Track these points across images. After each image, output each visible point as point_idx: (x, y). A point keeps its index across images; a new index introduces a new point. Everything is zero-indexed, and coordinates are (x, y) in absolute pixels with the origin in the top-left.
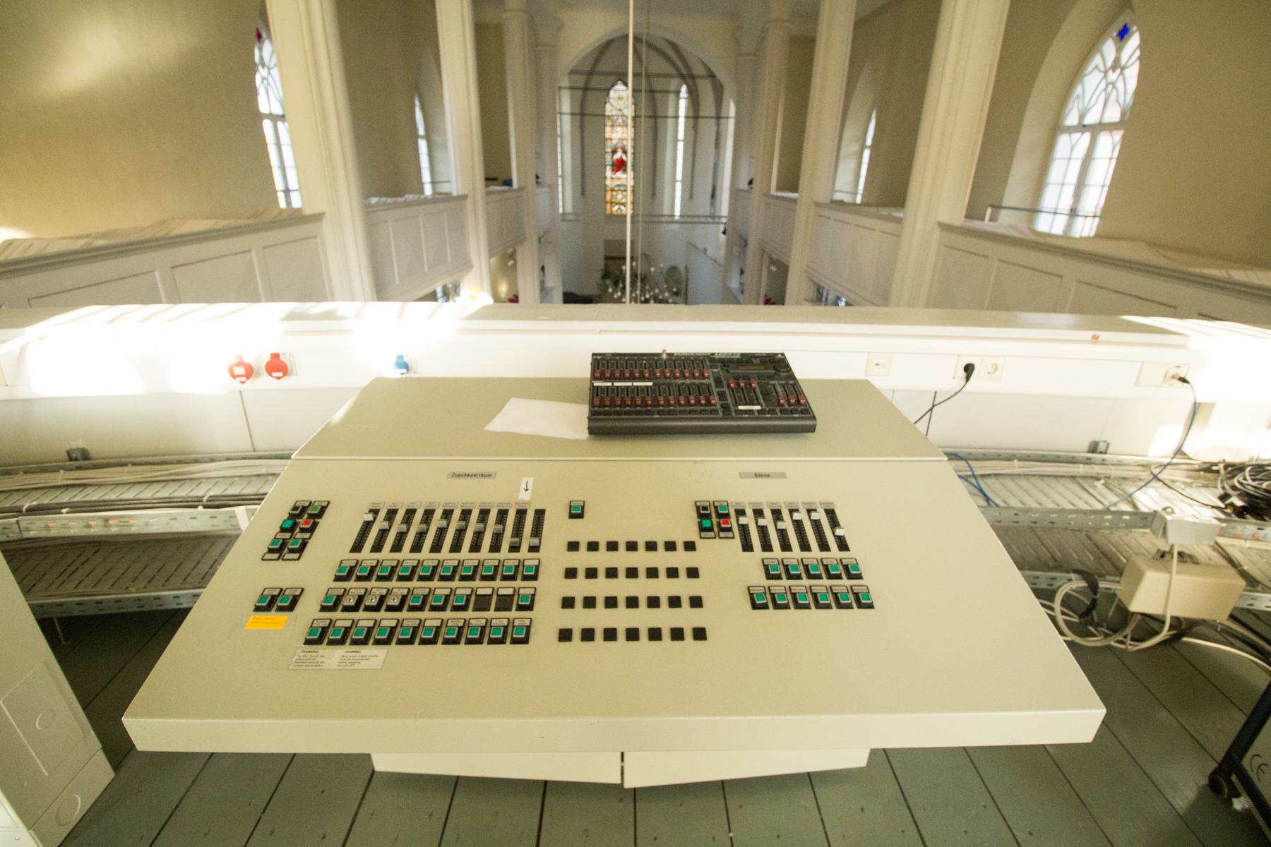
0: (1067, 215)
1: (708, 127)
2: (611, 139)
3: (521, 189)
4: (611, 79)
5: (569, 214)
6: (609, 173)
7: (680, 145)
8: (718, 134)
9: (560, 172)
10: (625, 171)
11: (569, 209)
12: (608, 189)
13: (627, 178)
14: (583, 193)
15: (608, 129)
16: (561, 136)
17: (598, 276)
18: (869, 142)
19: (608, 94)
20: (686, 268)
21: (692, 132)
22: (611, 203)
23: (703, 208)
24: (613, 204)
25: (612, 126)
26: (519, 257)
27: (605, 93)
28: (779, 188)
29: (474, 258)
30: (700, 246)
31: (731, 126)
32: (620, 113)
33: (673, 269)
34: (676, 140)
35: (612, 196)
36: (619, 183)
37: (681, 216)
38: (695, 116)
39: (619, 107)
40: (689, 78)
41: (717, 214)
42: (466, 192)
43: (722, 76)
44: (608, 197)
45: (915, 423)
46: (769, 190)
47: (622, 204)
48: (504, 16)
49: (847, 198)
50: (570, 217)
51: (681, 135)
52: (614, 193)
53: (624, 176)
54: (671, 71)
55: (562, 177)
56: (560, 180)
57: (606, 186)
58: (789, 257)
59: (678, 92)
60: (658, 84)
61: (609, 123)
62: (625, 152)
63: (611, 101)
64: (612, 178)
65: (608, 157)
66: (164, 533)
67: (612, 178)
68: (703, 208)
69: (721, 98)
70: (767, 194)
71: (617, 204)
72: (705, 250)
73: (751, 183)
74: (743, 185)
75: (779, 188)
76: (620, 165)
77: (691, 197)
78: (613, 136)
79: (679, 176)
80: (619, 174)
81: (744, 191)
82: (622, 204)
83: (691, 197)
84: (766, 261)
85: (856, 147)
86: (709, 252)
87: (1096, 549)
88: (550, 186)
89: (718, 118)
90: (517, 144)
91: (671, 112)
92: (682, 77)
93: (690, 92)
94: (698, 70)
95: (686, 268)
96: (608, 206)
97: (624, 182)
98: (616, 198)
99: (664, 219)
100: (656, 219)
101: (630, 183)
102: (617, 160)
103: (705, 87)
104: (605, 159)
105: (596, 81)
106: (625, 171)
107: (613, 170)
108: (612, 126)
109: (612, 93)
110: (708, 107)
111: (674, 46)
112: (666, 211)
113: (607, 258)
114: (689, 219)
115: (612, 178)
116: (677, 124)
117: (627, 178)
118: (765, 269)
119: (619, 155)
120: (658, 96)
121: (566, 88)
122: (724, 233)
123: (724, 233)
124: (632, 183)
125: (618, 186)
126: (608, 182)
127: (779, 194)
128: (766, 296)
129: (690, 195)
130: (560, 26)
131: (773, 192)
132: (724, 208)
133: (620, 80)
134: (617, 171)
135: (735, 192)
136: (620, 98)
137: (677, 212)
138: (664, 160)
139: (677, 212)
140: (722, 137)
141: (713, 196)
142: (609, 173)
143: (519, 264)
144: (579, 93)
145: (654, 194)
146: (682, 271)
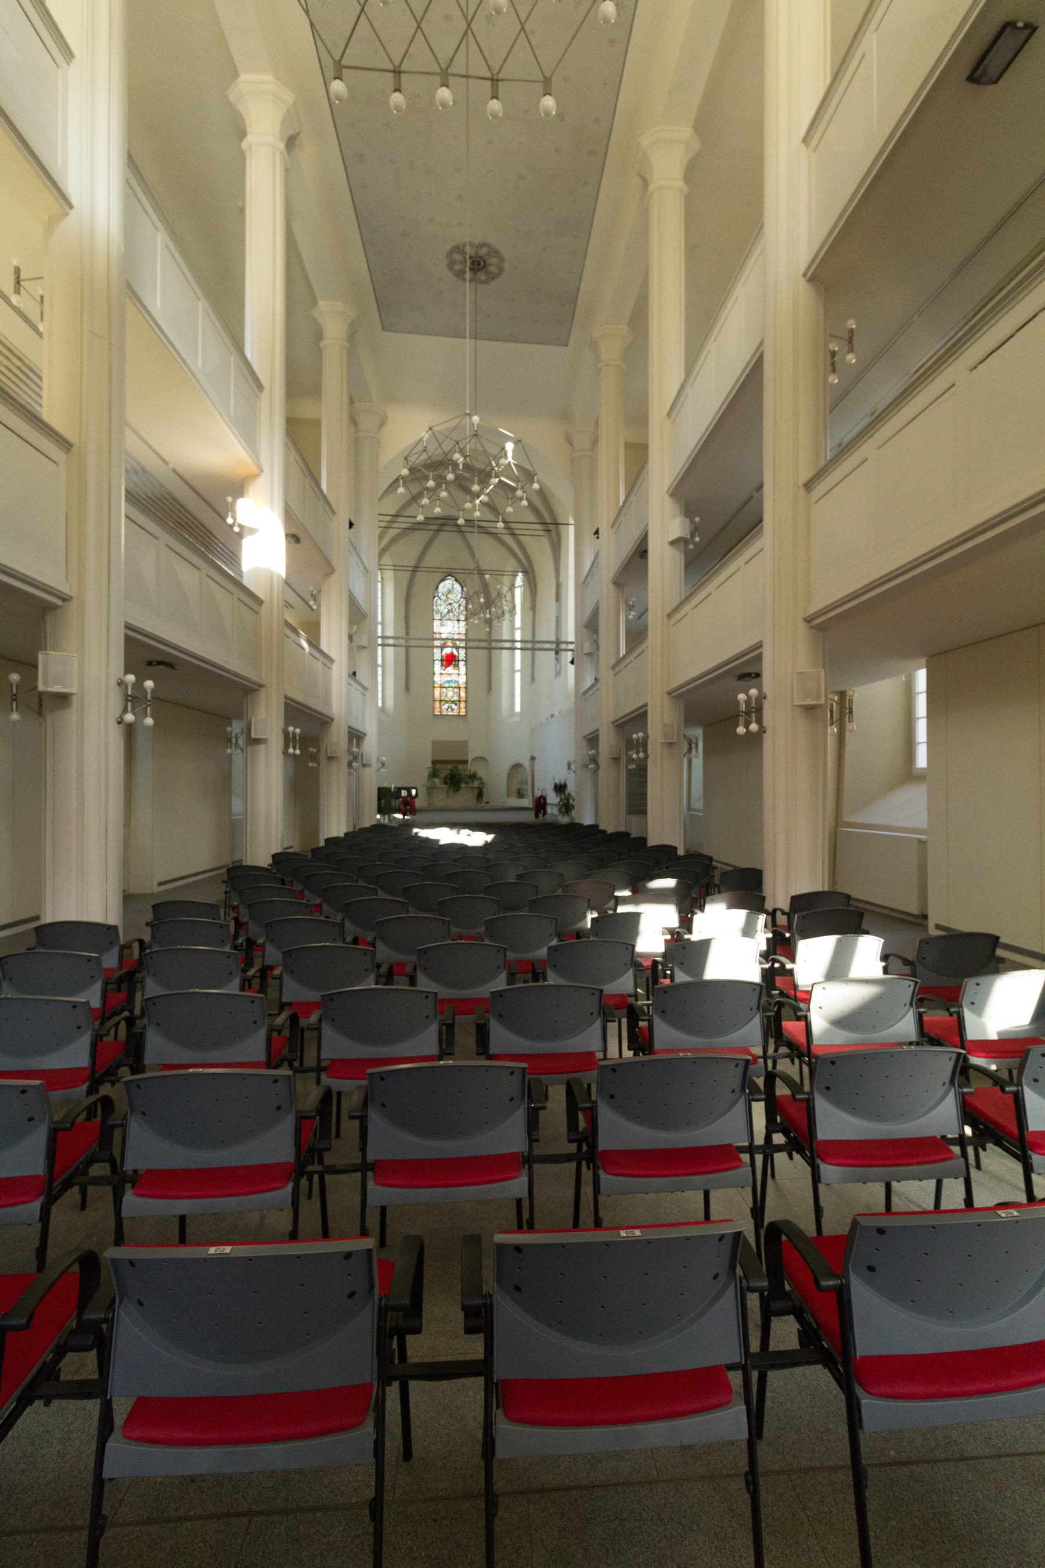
0: (919, 718)
6: (437, 667)
7: (518, 676)
8: (558, 587)
9: (380, 662)
10: (457, 666)
11: (390, 703)
12: (436, 685)
13: (459, 675)
14: (407, 688)
15: (436, 623)
16: (383, 666)
21: (531, 613)
22: (441, 701)
24: (443, 702)
33: (517, 767)
36: (449, 678)
37: (517, 575)
47: (453, 702)
51: (518, 666)
52: (444, 690)
53: (456, 672)
55: (383, 624)
61: (437, 617)
63: (440, 595)
67: (441, 675)
71: (447, 702)
76: (450, 660)
77: (533, 679)
78: (443, 630)
80: (450, 669)
82: (453, 702)
83: (533, 679)
90: (328, 476)
96: (437, 704)
97: (455, 678)
98: (446, 696)
101: (462, 679)
106: (457, 666)
107: (442, 665)
113: (434, 762)
115: (441, 675)
117: (459, 675)
119: (447, 651)
122: (572, 662)
123: (572, 662)
125: (448, 682)
126: (437, 678)
134: (446, 667)
140: (563, 589)
142: (437, 667)
145: (490, 689)
146: (526, 763)
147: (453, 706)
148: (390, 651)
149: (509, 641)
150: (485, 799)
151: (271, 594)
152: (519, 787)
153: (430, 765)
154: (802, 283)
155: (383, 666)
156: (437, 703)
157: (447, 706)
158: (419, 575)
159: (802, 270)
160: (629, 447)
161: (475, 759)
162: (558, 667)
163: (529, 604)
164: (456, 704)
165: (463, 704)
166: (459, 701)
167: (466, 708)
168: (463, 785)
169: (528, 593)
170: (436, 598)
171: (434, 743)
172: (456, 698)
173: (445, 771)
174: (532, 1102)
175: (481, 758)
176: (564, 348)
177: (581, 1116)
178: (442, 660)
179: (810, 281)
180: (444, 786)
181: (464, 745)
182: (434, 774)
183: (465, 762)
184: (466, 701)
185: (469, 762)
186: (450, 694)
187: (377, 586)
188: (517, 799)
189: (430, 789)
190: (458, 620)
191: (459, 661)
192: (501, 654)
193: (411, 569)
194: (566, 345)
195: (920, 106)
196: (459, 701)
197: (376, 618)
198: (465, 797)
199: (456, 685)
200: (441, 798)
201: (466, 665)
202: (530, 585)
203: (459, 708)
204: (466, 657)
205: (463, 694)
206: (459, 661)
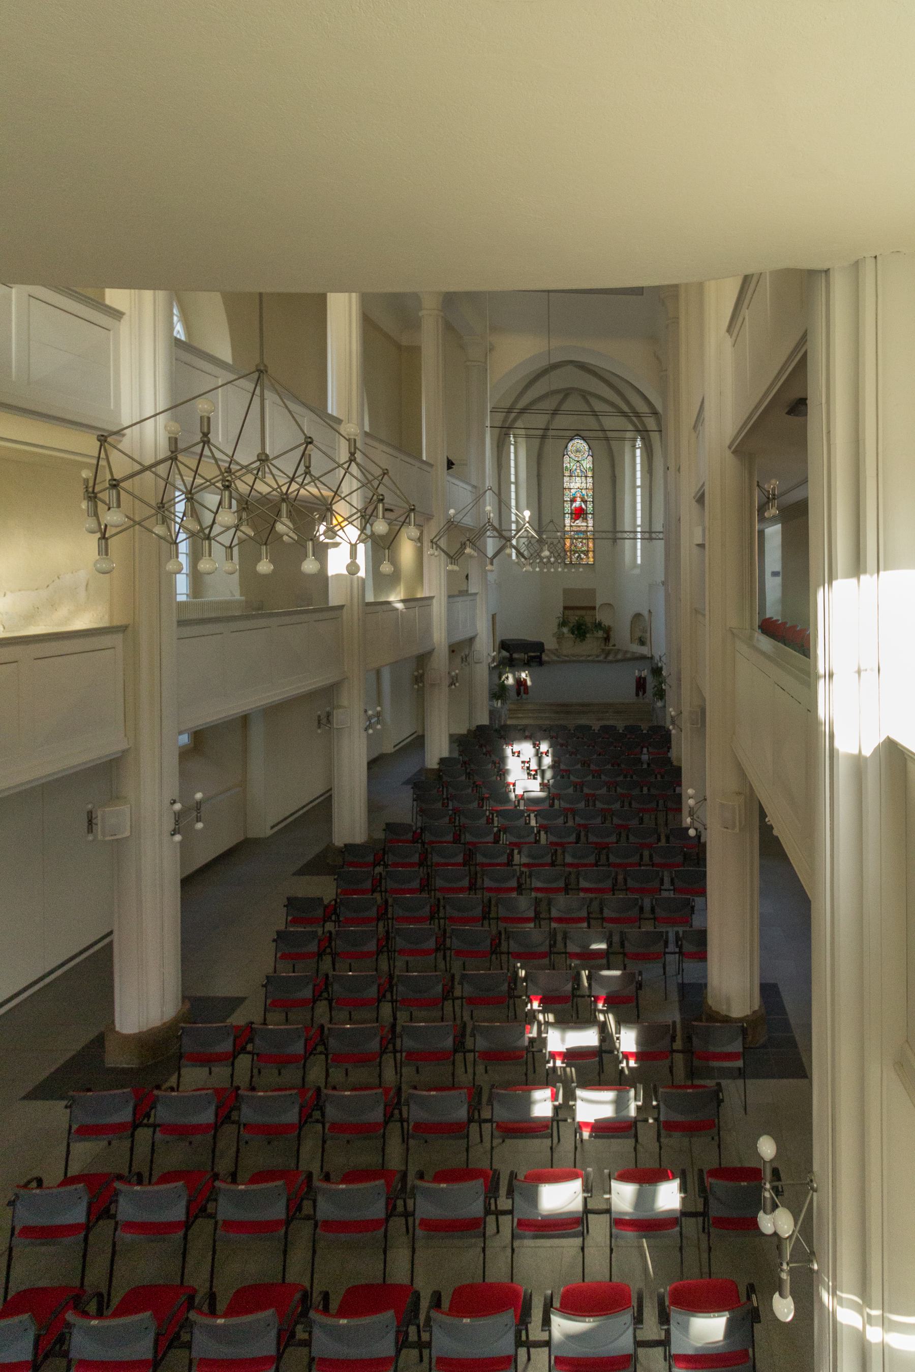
7: (639, 491)
10: (585, 519)
15: (566, 479)
17: (555, 622)
20: (650, 611)
21: (648, 475)
22: (571, 551)
33: (638, 616)
34: (634, 487)
35: (572, 544)
45: (583, 1280)
56: (513, 487)
59: (635, 440)
61: (567, 473)
62: (585, 502)
63: (569, 453)
65: (567, 505)
66: (561, 1214)
76: (579, 513)
78: (572, 485)
79: (639, 483)
80: (579, 522)
82: (582, 552)
87: (529, 1296)
95: (650, 611)
99: (626, 535)
102: (576, 509)
106: (585, 519)
107: (571, 518)
108: (571, 476)
112: (627, 527)
113: (565, 608)
119: (577, 504)
136: (578, 451)
142: (568, 521)
144: (537, 442)
146: (646, 613)
147: (582, 556)
150: (612, 642)
151: (352, 599)
153: (562, 609)
154: (728, 454)
155: (516, 483)
158: (549, 442)
159: (728, 442)
163: (646, 468)
164: (584, 554)
165: (591, 554)
167: (594, 557)
168: (588, 635)
169: (645, 454)
171: (566, 592)
172: (584, 548)
173: (573, 619)
175: (609, 604)
176: (640, 297)
177: (578, 1134)
178: (571, 514)
179: (733, 453)
180: (572, 636)
181: (592, 593)
182: (563, 623)
183: (594, 608)
184: (593, 551)
185: (597, 608)
187: (510, 448)
188: (639, 647)
189: (560, 637)
190: (586, 477)
191: (587, 514)
193: (552, 412)
194: (642, 295)
195: (768, 404)
198: (591, 646)
200: (570, 647)
201: (593, 518)
205: (591, 545)
206: (587, 514)
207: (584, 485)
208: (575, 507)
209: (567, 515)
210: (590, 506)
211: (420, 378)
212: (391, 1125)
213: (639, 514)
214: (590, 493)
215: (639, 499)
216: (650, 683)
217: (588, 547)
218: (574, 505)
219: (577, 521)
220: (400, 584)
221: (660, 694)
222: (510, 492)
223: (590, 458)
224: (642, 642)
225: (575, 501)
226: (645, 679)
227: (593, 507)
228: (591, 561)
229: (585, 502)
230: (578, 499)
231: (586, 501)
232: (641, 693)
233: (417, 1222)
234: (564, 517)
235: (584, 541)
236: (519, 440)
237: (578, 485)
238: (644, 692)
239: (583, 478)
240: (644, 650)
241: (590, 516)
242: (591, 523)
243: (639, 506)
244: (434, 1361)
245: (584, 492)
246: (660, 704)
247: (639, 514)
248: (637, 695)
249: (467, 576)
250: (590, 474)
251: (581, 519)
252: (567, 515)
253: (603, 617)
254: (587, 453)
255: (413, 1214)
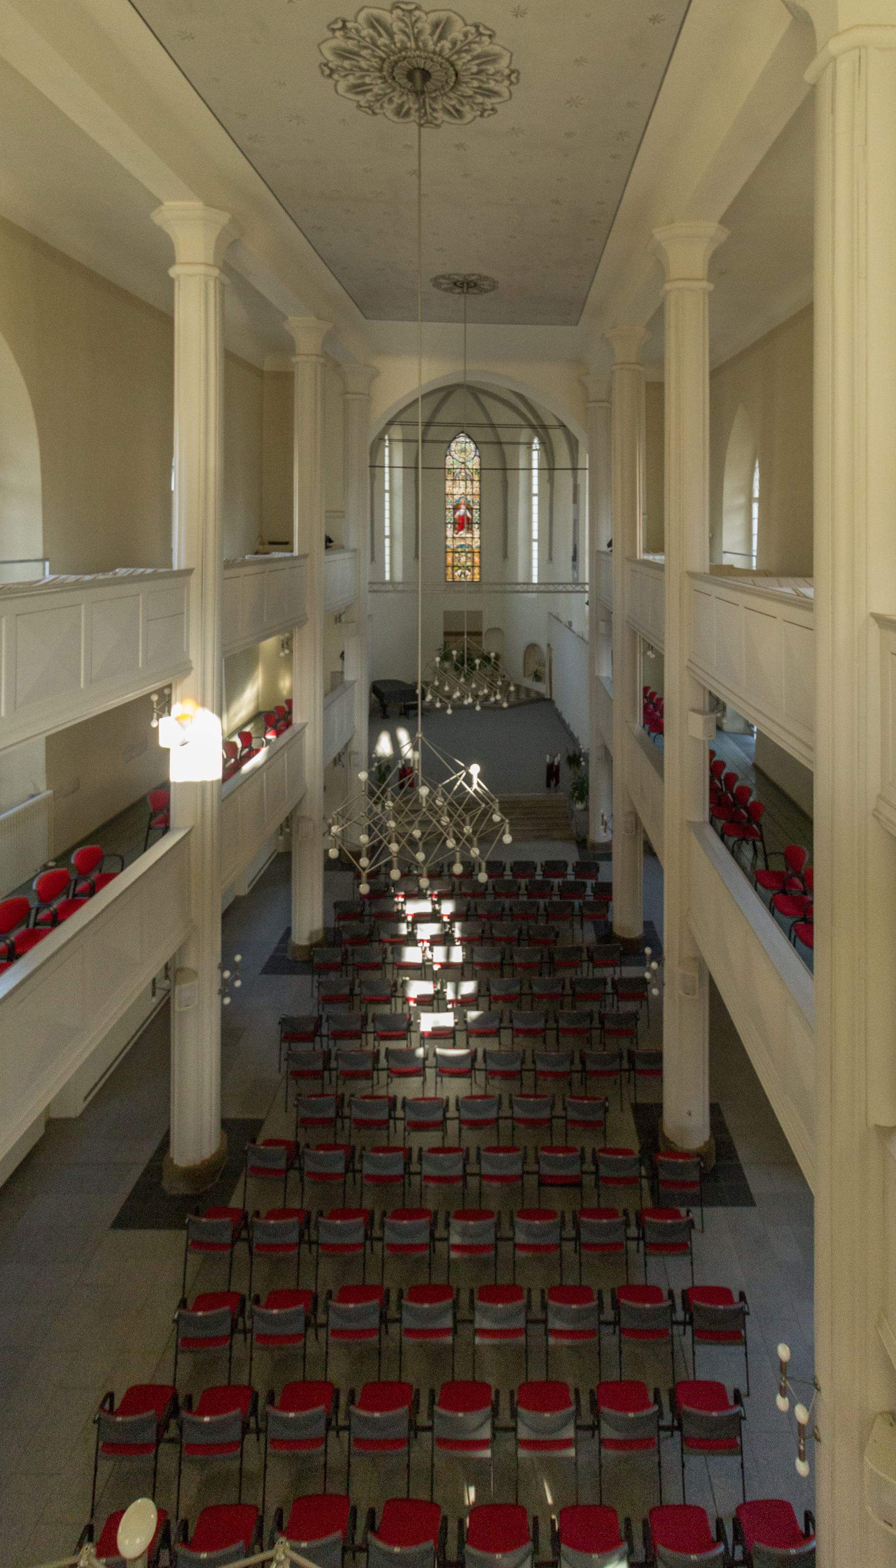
1: (564, 479)
2: (453, 495)
3: (303, 556)
4: (453, 430)
5: (399, 583)
7: (535, 545)
8: (576, 487)
10: (470, 530)
11: (399, 577)
13: (473, 538)
16: (391, 491)
18: (756, 494)
19: (449, 446)
20: (549, 645)
21: (548, 485)
22: (453, 567)
23: (565, 573)
25: (454, 480)
26: (296, 644)
27: (445, 445)
28: (647, 550)
29: (194, 655)
30: (564, 619)
31: (585, 479)
32: (463, 466)
34: (530, 495)
38: (549, 468)
39: (461, 460)
40: (540, 428)
41: (581, 581)
42: (191, 566)
43: (574, 428)
44: (449, 559)
46: (635, 553)
47: (467, 568)
48: (294, 360)
49: (738, 562)
50: (400, 587)
52: (457, 555)
53: (470, 535)
54: (519, 421)
56: (387, 496)
57: (446, 547)
58: (663, 642)
59: (530, 444)
60: (505, 435)
61: (449, 477)
62: (470, 509)
63: (453, 453)
64: (454, 538)
65: (449, 514)
67: (453, 538)
68: (565, 573)
69: (577, 452)
70: (632, 559)
71: (460, 568)
72: (570, 623)
73: (610, 545)
74: (604, 547)
75: (647, 550)
76: (462, 524)
77: (551, 558)
78: (455, 491)
79: (535, 490)
80: (462, 533)
81: (603, 553)
82: (467, 568)
83: (551, 558)
84: (640, 648)
85: (741, 500)
86: (574, 628)
88: (354, 550)
89: (575, 469)
91: (522, 464)
92: (532, 427)
93: (542, 443)
94: (549, 421)
95: (549, 645)
97: (469, 542)
98: (459, 561)
100: (509, 588)
101: (476, 543)
103: (557, 436)
104: (445, 516)
105: (434, 433)
106: (470, 530)
107: (454, 529)
108: (454, 480)
109: (453, 445)
110: (563, 458)
111: (521, 397)
113: (447, 634)
114: (548, 587)
115: (453, 538)
116: (530, 478)
117: (473, 538)
118: (639, 658)
119: (461, 512)
120: (506, 448)
121: (399, 441)
123: (587, 603)
124: (478, 544)
125: (461, 546)
126: (449, 543)
127: (651, 557)
128: (646, 689)
129: (549, 555)
130: (375, 374)
131: (641, 555)
132: (586, 575)
133: (463, 432)
135: (596, 554)
137: (535, 580)
138: (516, 520)
139: (535, 580)
141: (575, 558)
142: (449, 533)
143: (296, 654)
145: (505, 556)
146: (544, 648)
147: (467, 572)
148: (521, 578)
149: (524, 584)
152: (536, 667)
155: (391, 491)
156: (450, 569)
157: (459, 572)
160: (649, 385)
161: (489, 630)
162: (575, 576)
164: (469, 570)
165: (477, 570)
166: (473, 567)
167: (480, 574)
170: (449, 457)
172: (469, 564)
174: (541, 1184)
181: (477, 616)
183: (479, 634)
184: (480, 567)
186: (463, 559)
187: (384, 497)
190: (472, 480)
191: (472, 523)
192: (518, 475)
196: (473, 567)
197: (384, 531)
199: (470, 549)
201: (480, 528)
202: (547, 454)
203: (473, 574)
204: (480, 519)
205: (477, 559)
206: (472, 523)
207: (469, 490)
208: (459, 516)
209: (449, 526)
210: (476, 515)
211: (292, 439)
212: (236, 1335)
213: (535, 526)
214: (477, 499)
215: (535, 509)
216: (566, 774)
217: (473, 561)
218: (458, 514)
219: (461, 532)
220: (257, 664)
221: (581, 791)
222: (384, 501)
223: (477, 459)
224: (538, 677)
225: (459, 509)
226: (558, 767)
227: (480, 516)
228: (477, 578)
229: (470, 509)
230: (463, 507)
231: (472, 509)
232: (553, 783)
233: (254, 1337)
234: (446, 527)
235: (469, 555)
236: (395, 444)
237: (462, 490)
238: (557, 782)
239: (469, 483)
240: (541, 688)
241: (476, 526)
242: (477, 533)
243: (535, 518)
244: (269, 1441)
245: (469, 498)
246: (579, 806)
247: (535, 526)
248: (548, 785)
249: (342, 655)
250: (476, 478)
251: (465, 530)
252: (449, 526)
253: (490, 647)
254: (473, 454)
255: (251, 1331)
